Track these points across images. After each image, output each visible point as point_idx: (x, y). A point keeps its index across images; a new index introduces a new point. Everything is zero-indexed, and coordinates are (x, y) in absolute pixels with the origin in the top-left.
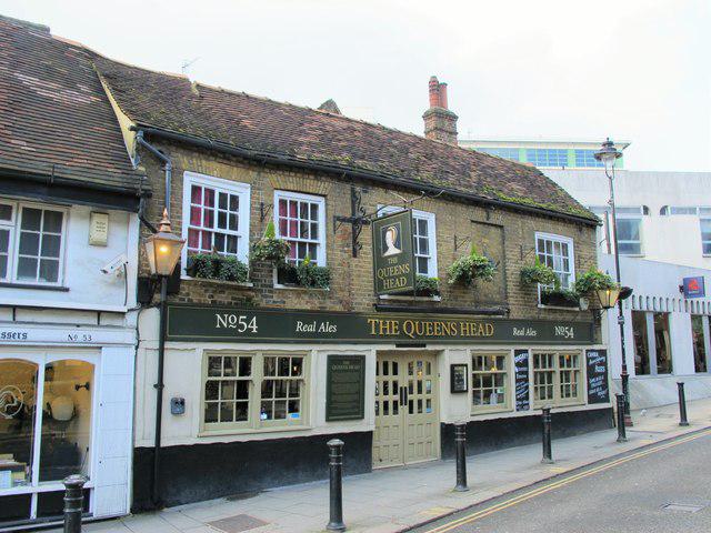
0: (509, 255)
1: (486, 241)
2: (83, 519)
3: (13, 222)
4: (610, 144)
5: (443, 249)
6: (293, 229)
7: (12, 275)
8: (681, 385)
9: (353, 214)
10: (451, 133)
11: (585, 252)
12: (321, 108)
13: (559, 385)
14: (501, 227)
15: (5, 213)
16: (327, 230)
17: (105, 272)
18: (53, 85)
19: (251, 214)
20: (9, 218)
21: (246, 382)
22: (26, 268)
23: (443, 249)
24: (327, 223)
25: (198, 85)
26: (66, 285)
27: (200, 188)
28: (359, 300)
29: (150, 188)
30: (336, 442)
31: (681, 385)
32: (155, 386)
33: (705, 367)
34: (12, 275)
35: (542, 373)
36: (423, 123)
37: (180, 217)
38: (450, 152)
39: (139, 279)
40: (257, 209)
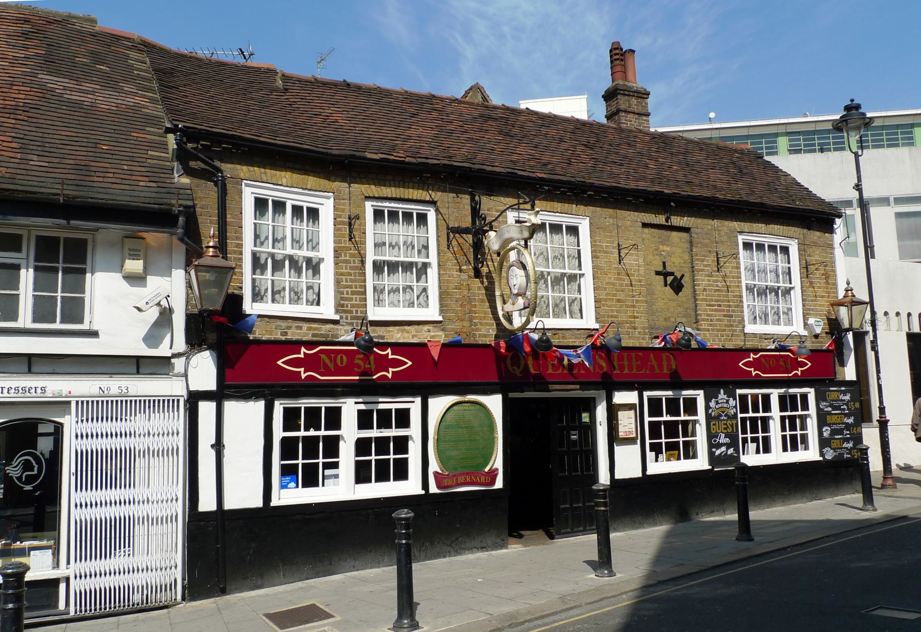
0: (699, 265)
1: (665, 248)
2: (26, 622)
3: (23, 254)
4: (858, 107)
5: (602, 262)
6: (773, 363)
7: (25, 319)
8: (171, 348)
9: (474, 222)
10: (640, 114)
11: (816, 256)
12: (465, 96)
13: (780, 434)
14: (686, 230)
15: (13, 243)
16: (438, 245)
17: (139, 309)
18: (88, 86)
19: (336, 230)
20: (19, 250)
21: (768, 417)
22: (43, 311)
23: (602, 262)
24: (438, 236)
25: (283, 75)
26: (95, 327)
27: (301, 208)
28: (483, 332)
29: (190, 203)
30: (404, 513)
31: (171, 348)
32: (212, 446)
33: (798, 151)
34: (25, 319)
35: (754, 420)
36: (603, 104)
37: (241, 239)
38: (631, 137)
39: (187, 315)
40: (342, 223)
